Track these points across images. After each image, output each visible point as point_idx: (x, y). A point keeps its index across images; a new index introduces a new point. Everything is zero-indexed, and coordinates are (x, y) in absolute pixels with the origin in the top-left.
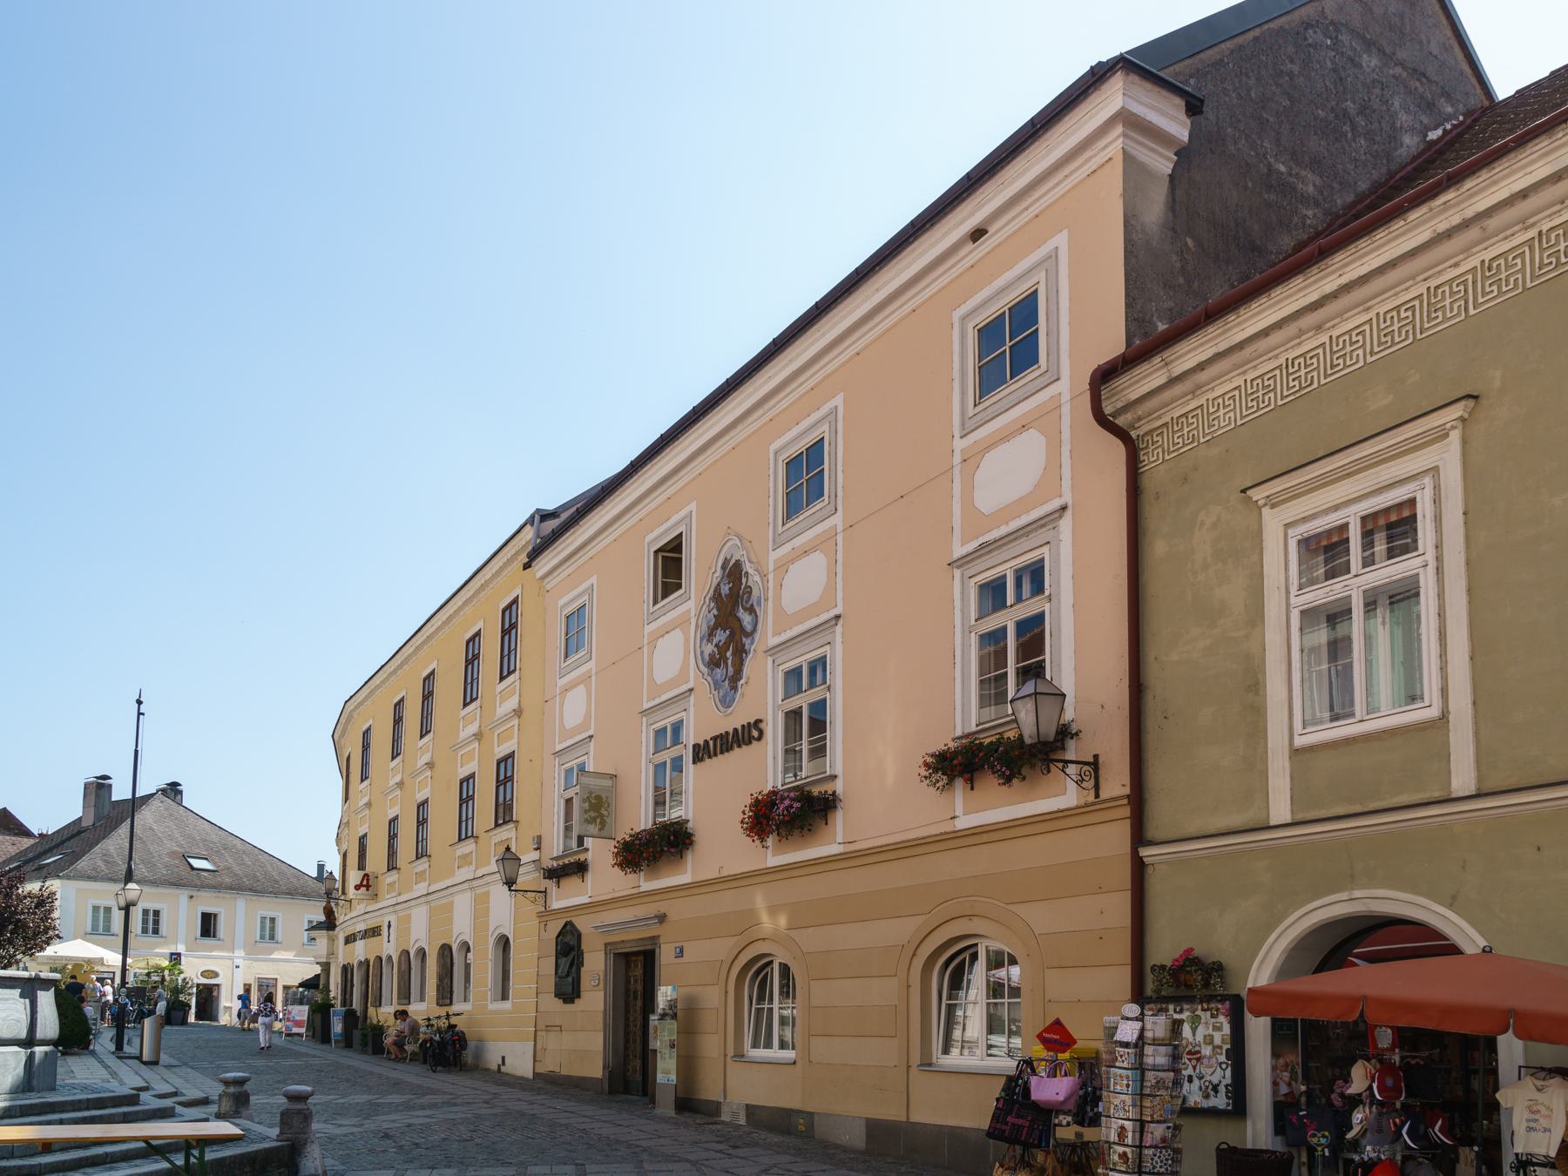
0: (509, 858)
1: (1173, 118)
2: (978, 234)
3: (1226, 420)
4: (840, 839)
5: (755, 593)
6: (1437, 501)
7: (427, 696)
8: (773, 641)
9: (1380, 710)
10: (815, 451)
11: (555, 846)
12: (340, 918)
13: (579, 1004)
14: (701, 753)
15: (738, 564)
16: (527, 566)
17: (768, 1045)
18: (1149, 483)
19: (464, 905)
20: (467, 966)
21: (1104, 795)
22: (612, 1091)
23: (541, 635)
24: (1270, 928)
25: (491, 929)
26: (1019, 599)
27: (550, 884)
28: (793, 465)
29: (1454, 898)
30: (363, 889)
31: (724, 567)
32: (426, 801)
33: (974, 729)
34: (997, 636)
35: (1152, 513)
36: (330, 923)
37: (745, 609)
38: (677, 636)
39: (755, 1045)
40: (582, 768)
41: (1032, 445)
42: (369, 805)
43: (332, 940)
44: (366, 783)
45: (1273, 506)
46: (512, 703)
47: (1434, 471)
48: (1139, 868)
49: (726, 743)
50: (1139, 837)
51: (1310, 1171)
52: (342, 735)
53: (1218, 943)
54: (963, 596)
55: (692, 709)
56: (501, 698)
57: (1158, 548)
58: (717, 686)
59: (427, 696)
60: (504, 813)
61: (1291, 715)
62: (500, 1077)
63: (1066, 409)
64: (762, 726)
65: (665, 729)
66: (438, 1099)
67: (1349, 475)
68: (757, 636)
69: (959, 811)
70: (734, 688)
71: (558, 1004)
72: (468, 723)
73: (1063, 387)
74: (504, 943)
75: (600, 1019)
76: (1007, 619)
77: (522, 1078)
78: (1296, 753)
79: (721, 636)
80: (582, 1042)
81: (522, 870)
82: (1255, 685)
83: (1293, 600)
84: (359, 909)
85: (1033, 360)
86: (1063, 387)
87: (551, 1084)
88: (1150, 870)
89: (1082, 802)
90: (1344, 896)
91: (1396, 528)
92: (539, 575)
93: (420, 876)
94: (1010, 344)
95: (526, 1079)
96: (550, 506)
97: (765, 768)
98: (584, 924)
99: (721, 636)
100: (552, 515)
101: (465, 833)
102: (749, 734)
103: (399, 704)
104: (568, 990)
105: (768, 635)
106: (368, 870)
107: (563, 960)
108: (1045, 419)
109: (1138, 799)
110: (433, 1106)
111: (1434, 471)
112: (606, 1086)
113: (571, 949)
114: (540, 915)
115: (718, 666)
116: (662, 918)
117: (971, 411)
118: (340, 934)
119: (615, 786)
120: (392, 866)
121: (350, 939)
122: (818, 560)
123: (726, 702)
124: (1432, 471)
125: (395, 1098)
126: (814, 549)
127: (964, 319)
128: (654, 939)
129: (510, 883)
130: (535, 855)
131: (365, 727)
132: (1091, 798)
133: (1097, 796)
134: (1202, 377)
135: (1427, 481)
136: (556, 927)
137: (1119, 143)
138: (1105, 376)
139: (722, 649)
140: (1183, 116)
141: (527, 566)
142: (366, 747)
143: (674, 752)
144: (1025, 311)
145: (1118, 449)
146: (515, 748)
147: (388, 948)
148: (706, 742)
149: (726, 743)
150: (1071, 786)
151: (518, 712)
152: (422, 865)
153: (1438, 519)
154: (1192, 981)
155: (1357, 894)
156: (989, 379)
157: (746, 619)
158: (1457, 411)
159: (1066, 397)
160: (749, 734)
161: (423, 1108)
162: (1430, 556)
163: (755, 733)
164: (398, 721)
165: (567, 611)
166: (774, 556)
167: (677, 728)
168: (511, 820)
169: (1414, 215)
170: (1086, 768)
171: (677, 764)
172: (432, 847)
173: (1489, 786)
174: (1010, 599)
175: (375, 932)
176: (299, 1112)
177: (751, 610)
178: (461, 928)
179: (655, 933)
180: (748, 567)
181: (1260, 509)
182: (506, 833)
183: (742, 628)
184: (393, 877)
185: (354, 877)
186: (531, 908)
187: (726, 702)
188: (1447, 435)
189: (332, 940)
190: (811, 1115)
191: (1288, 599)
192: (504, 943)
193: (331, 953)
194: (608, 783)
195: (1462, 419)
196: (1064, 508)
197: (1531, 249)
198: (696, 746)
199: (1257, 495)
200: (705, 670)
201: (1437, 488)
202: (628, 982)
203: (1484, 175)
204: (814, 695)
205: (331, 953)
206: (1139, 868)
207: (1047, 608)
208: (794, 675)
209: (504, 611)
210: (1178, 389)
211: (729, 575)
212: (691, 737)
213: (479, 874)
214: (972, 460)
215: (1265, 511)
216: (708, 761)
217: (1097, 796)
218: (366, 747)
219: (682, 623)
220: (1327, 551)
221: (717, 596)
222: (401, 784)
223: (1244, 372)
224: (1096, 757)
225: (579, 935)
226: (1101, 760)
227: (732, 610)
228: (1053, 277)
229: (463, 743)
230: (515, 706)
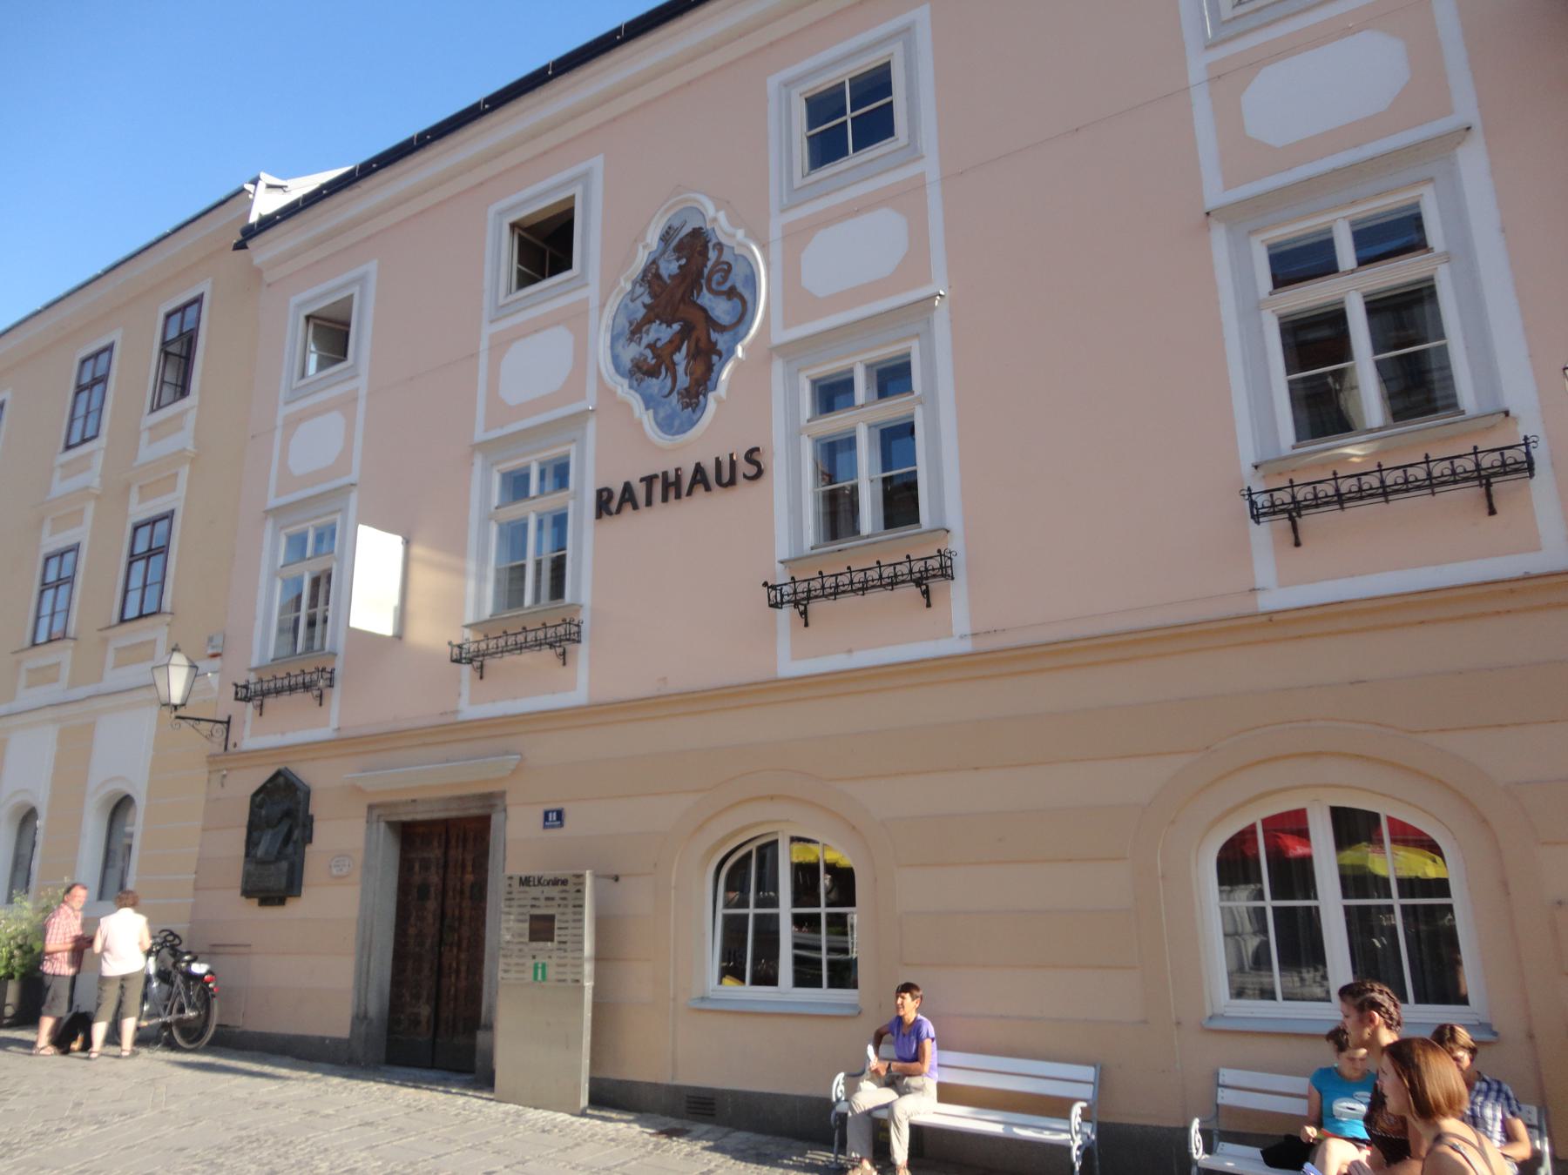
17: (766, 978)
26: (542, 491)
51: (1390, 1144)
63: (362, 406)
76: (530, 511)
79: (661, 333)
94: (546, 247)
95: (337, 1042)
117: (798, 181)
156: (826, 149)
157: (721, 309)
159: (363, 392)
177: (732, 293)
204: (317, 566)
211: (679, 249)
212: (585, 484)
214: (500, 346)
221: (651, 277)
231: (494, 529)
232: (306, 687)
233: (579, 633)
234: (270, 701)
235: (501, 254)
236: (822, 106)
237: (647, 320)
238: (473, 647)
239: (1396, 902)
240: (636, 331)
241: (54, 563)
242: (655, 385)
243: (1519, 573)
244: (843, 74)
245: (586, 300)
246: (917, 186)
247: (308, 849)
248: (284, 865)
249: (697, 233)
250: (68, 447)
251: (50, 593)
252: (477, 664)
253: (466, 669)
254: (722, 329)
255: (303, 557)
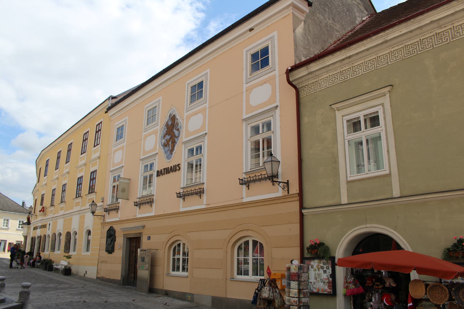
0: (93, 204)
1: (305, 7)
2: (251, 30)
3: (324, 85)
4: (205, 203)
5: (179, 125)
6: (384, 112)
7: (69, 150)
8: (184, 140)
9: (370, 171)
10: (200, 85)
11: (109, 201)
12: (32, 221)
13: (113, 254)
14: (159, 174)
15: (174, 116)
16: (106, 112)
18: (302, 101)
19: (77, 218)
20: (75, 240)
21: (290, 193)
22: (124, 284)
23: (109, 133)
24: (342, 235)
25: (85, 226)
26: (263, 132)
27: (106, 214)
28: (193, 88)
29: (396, 227)
30: (42, 212)
31: (170, 116)
32: (66, 184)
33: (249, 170)
34: (257, 143)
35: (303, 111)
36: (29, 223)
37: (176, 129)
38: (153, 136)
39: (174, 270)
40: (119, 176)
41: (267, 88)
42: (46, 184)
43: (29, 228)
44: (46, 177)
45: (338, 111)
46: (98, 154)
47: (383, 105)
48: (302, 216)
49: (168, 171)
50: (302, 207)
52: (39, 162)
53: (328, 240)
54: (246, 130)
55: (123, 172)
56: (94, 153)
57: (305, 120)
58: (166, 152)
59: (69, 150)
60: (92, 190)
61: (347, 171)
62: (84, 278)
64: (180, 166)
65: (147, 165)
66: (66, 286)
67: (359, 104)
68: (180, 138)
69: (244, 196)
70: (171, 154)
71: (106, 254)
72: (83, 160)
73: (276, 73)
74: (89, 233)
75: (121, 260)
77: (91, 279)
78: (348, 182)
79: (168, 137)
80: (115, 267)
81: (97, 208)
82: (335, 161)
83: (345, 137)
84: (40, 218)
85: (201, 96)
86: (276, 73)
87: (102, 281)
88: (305, 217)
89: (284, 195)
90: (364, 226)
91: (374, 120)
92: (110, 115)
93: (62, 209)
95: (94, 279)
96: (115, 95)
97: (182, 179)
98: (117, 228)
99: (168, 137)
100: (115, 98)
101: (78, 195)
102: (176, 168)
103: (59, 153)
104: (110, 249)
105: (183, 137)
106: (44, 205)
107: (109, 239)
108: (271, 81)
109: (301, 194)
110: (65, 288)
111: (383, 105)
112: (122, 282)
113: (112, 235)
114: (102, 224)
115: (166, 146)
116: (144, 227)
117: (249, 77)
118: (32, 226)
119: (129, 184)
120: (52, 205)
121: (35, 228)
122: (200, 116)
123: (169, 158)
124: (382, 106)
125: (51, 285)
126: (199, 113)
127: (247, 51)
128: (141, 233)
129: (93, 213)
130: (102, 204)
131: (47, 159)
132: (286, 193)
133: (288, 193)
134: (317, 73)
135: (381, 107)
136: (107, 228)
137: (291, 11)
138: (289, 72)
139: (168, 141)
140: (307, 6)
141: (106, 112)
142: (47, 165)
143: (150, 172)
144: (265, 51)
145: (294, 90)
146: (97, 169)
147: (49, 232)
148: (161, 170)
149: (168, 171)
150: (280, 189)
151: (99, 158)
152: (63, 205)
153: (385, 118)
154: (317, 251)
155: (368, 226)
156: (255, 68)
157: (176, 133)
158: (388, 89)
159: (277, 75)
160: (176, 168)
161: (61, 289)
162: (383, 128)
163: (178, 168)
164: (59, 158)
165: (118, 127)
166: (144, 134)
167: (152, 165)
168: (94, 192)
169: (373, 38)
170: (285, 184)
171: (151, 176)
172: (66, 199)
173: (405, 193)
174: (261, 132)
175: (44, 226)
176: (26, 292)
177: (178, 130)
178: (74, 226)
179: (141, 232)
180: (177, 117)
181: (335, 111)
182: (93, 196)
183: (175, 135)
184: (52, 208)
185: (39, 208)
186: (99, 221)
187: (169, 158)
188: (385, 95)
189: (29, 228)
190: (193, 294)
191: (344, 137)
192: (89, 233)
193: (28, 233)
194: (128, 181)
195: (389, 91)
196: (277, 106)
197: (451, 31)
198: (158, 172)
199: (334, 107)
200: (162, 147)
201: (384, 109)
202: (130, 247)
203: (391, 30)
204: (150, 172)
205: (28, 233)
206: (302, 216)
207: (272, 135)
208: (191, 151)
209: (97, 126)
210: (310, 76)
211: (171, 119)
212: (156, 168)
213: (82, 209)
214: (249, 90)
215: (336, 111)
216: (161, 176)
217: (288, 193)
218: (47, 165)
219: (155, 133)
220: (355, 125)
221: (167, 125)
222: (55, 180)
223: (365, 59)
224: (288, 181)
225: (115, 231)
226: (289, 182)
227: (171, 130)
228: (273, 43)
229: (80, 166)
230: (98, 155)
231: (249, 143)
232: (148, 203)
233: (203, 191)
234: (110, 212)
235: (247, 62)
236: (254, 56)
237: (166, 134)
238: (246, 180)
239: (186, 257)
240: (164, 136)
241: (92, 174)
242: (167, 148)
243: (275, 197)
244: (259, 48)
245: (275, 75)
246: (274, 77)
247: (116, 243)
248: (111, 246)
249: (174, 116)
250: (95, 146)
251: (92, 181)
252: (247, 185)
253: (244, 187)
254: (177, 137)
255: (193, 155)
